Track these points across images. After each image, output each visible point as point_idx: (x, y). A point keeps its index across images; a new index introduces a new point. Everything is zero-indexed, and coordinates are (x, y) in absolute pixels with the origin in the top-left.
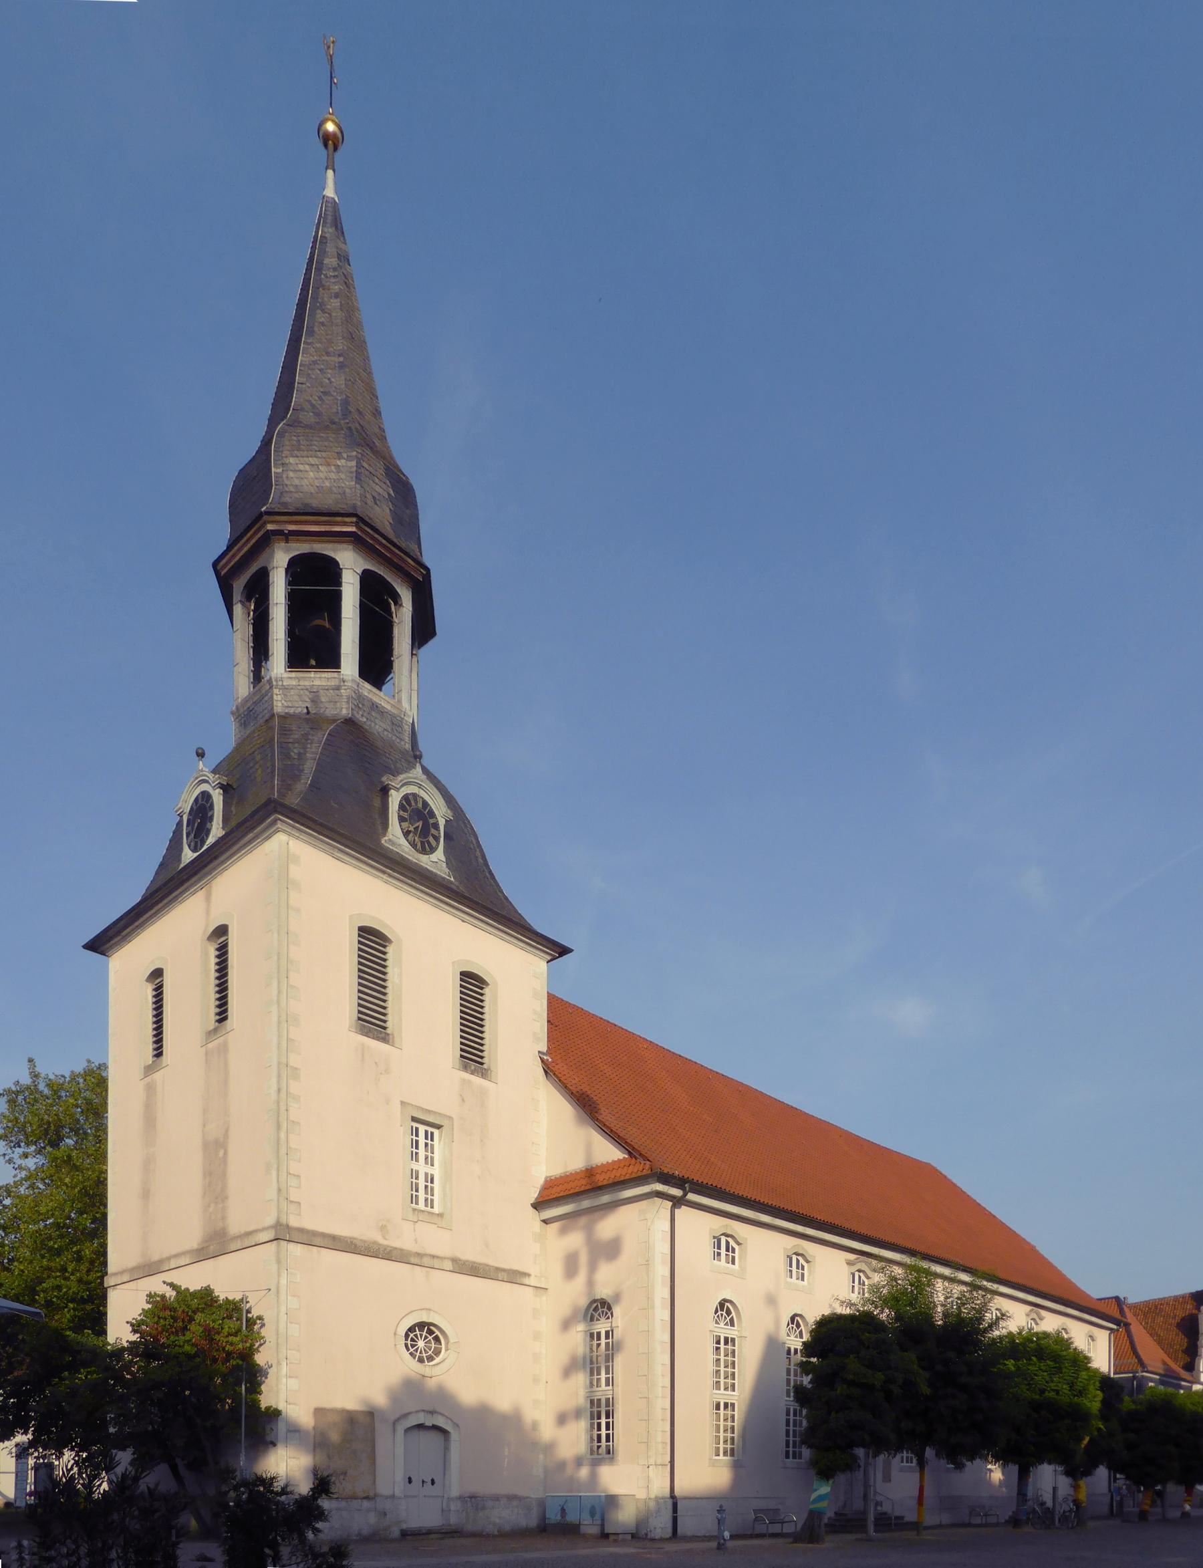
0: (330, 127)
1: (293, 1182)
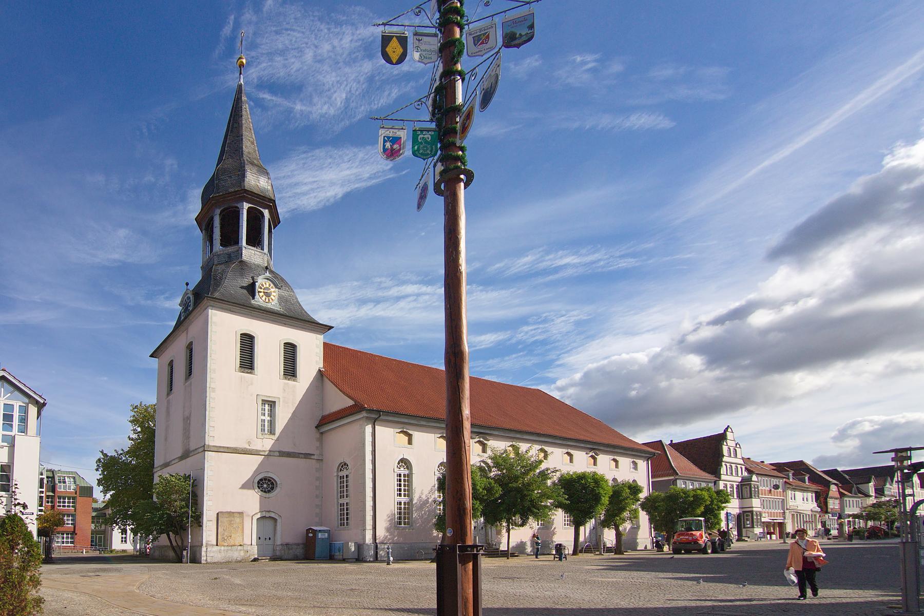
0: (244, 61)
1: (211, 429)
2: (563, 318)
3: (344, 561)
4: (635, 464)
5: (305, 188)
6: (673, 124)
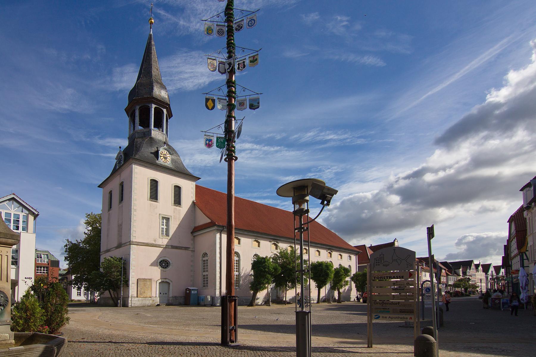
1: (134, 232)
2: (329, 170)
3: (205, 306)
4: (350, 257)
5: (186, 76)
6: (385, 64)
